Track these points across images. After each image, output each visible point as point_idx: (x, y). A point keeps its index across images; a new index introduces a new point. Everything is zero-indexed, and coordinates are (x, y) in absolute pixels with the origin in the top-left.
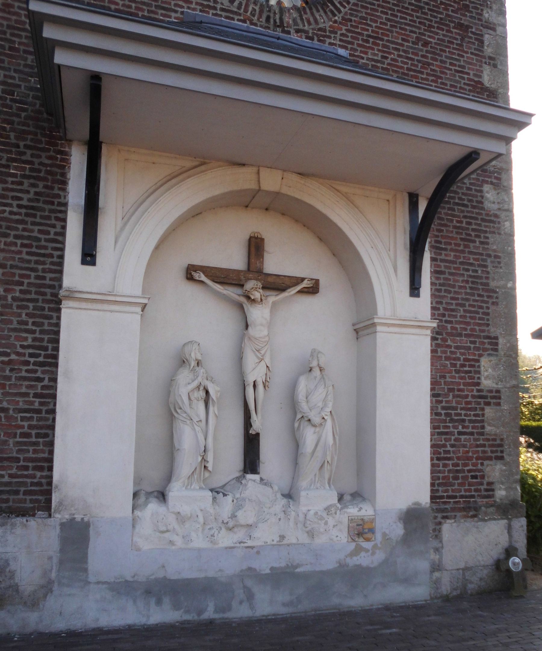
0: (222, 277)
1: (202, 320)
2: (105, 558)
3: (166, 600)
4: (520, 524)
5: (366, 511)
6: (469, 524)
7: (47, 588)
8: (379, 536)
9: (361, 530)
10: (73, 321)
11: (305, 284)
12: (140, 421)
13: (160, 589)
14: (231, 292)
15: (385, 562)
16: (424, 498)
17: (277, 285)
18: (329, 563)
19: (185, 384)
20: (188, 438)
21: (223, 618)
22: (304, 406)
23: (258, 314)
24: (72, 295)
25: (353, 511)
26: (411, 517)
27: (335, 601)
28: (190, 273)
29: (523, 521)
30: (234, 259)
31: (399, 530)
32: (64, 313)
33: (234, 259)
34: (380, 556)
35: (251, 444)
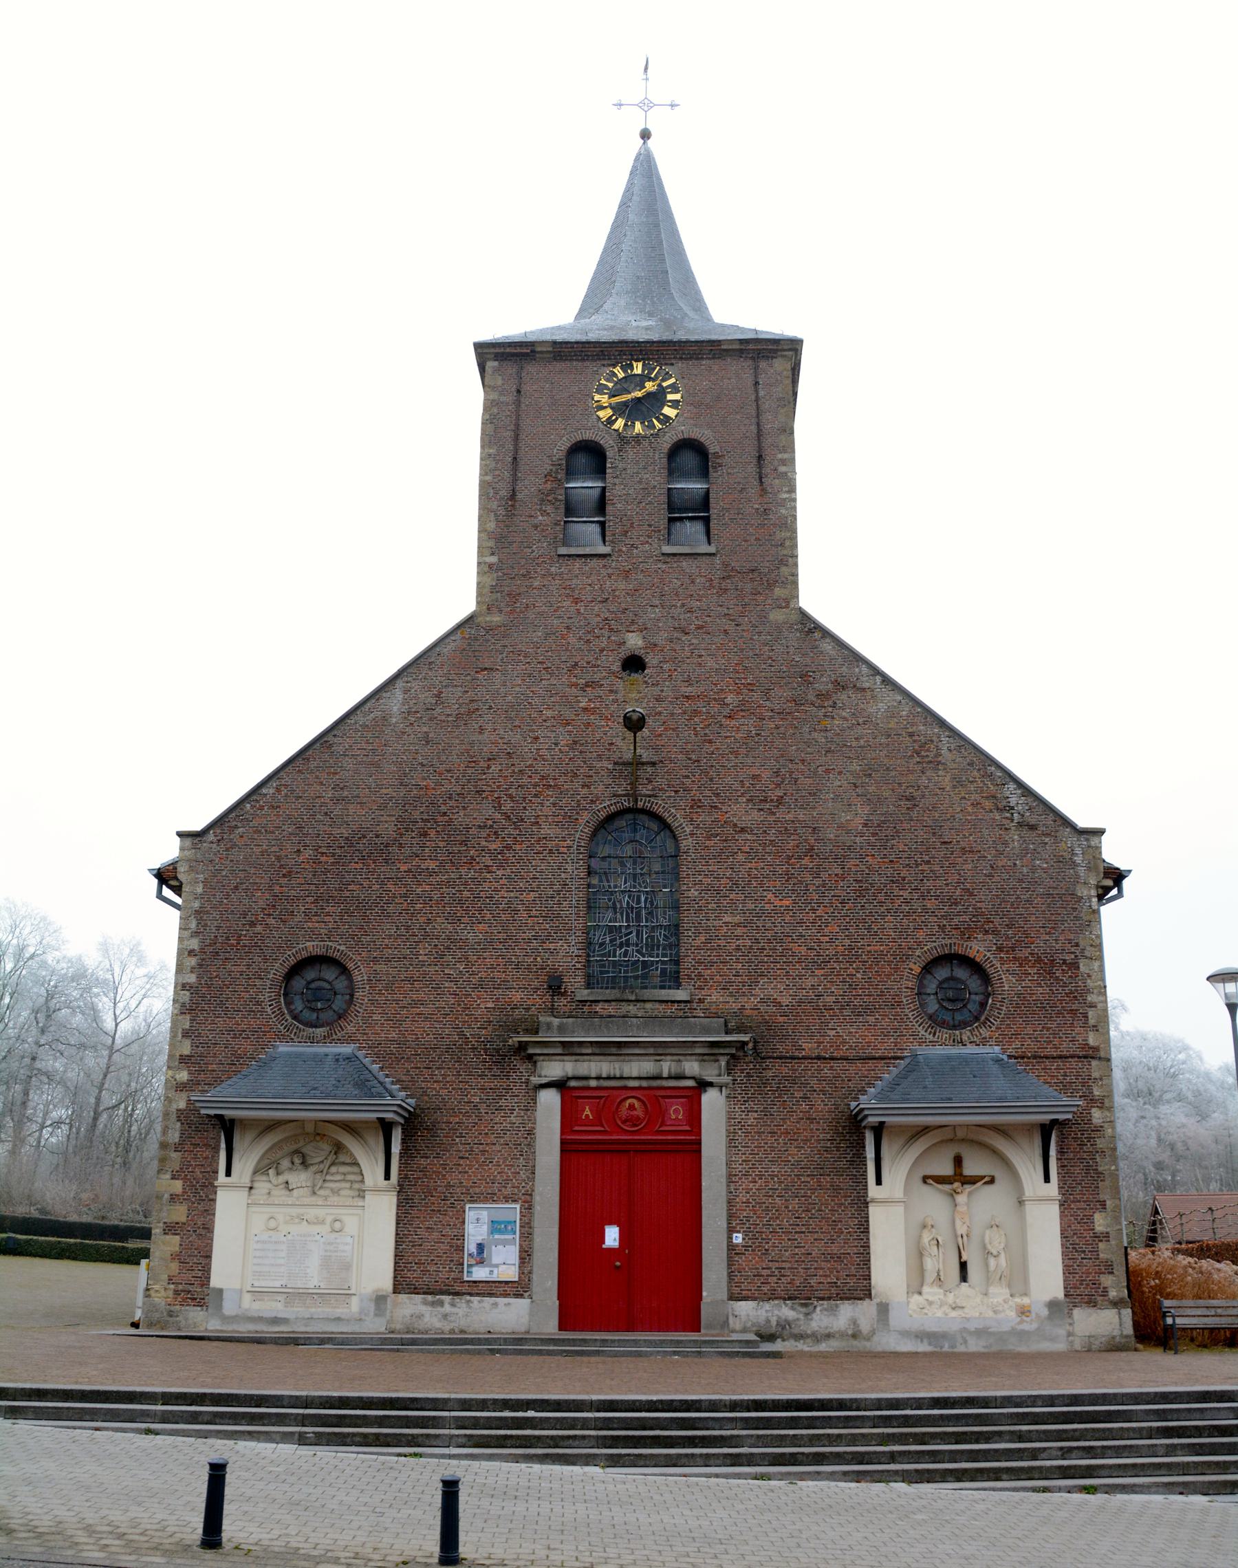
0: (940, 1180)
1: (933, 1202)
2: (897, 1319)
3: (925, 1341)
4: (1127, 1313)
5: (1026, 1301)
6: (1091, 1310)
7: (873, 1332)
8: (1033, 1315)
9: (1023, 1311)
10: (874, 1212)
11: (986, 1179)
12: (907, 1259)
13: (921, 1336)
14: (947, 1187)
15: (1038, 1329)
16: (1060, 1295)
17: (973, 1180)
18: (1006, 1328)
19: (926, 1237)
20: (929, 1264)
21: (312, 1040)
22: (989, 1247)
23: (961, 1199)
24: (873, 1201)
25: (1018, 1300)
26: (1053, 1305)
27: (1011, 1347)
28: (925, 1179)
29: (1129, 1311)
30: (947, 1169)
31: (1045, 1312)
32: (871, 1209)
33: (947, 1169)
34: (1034, 1326)
35: (963, 1266)
